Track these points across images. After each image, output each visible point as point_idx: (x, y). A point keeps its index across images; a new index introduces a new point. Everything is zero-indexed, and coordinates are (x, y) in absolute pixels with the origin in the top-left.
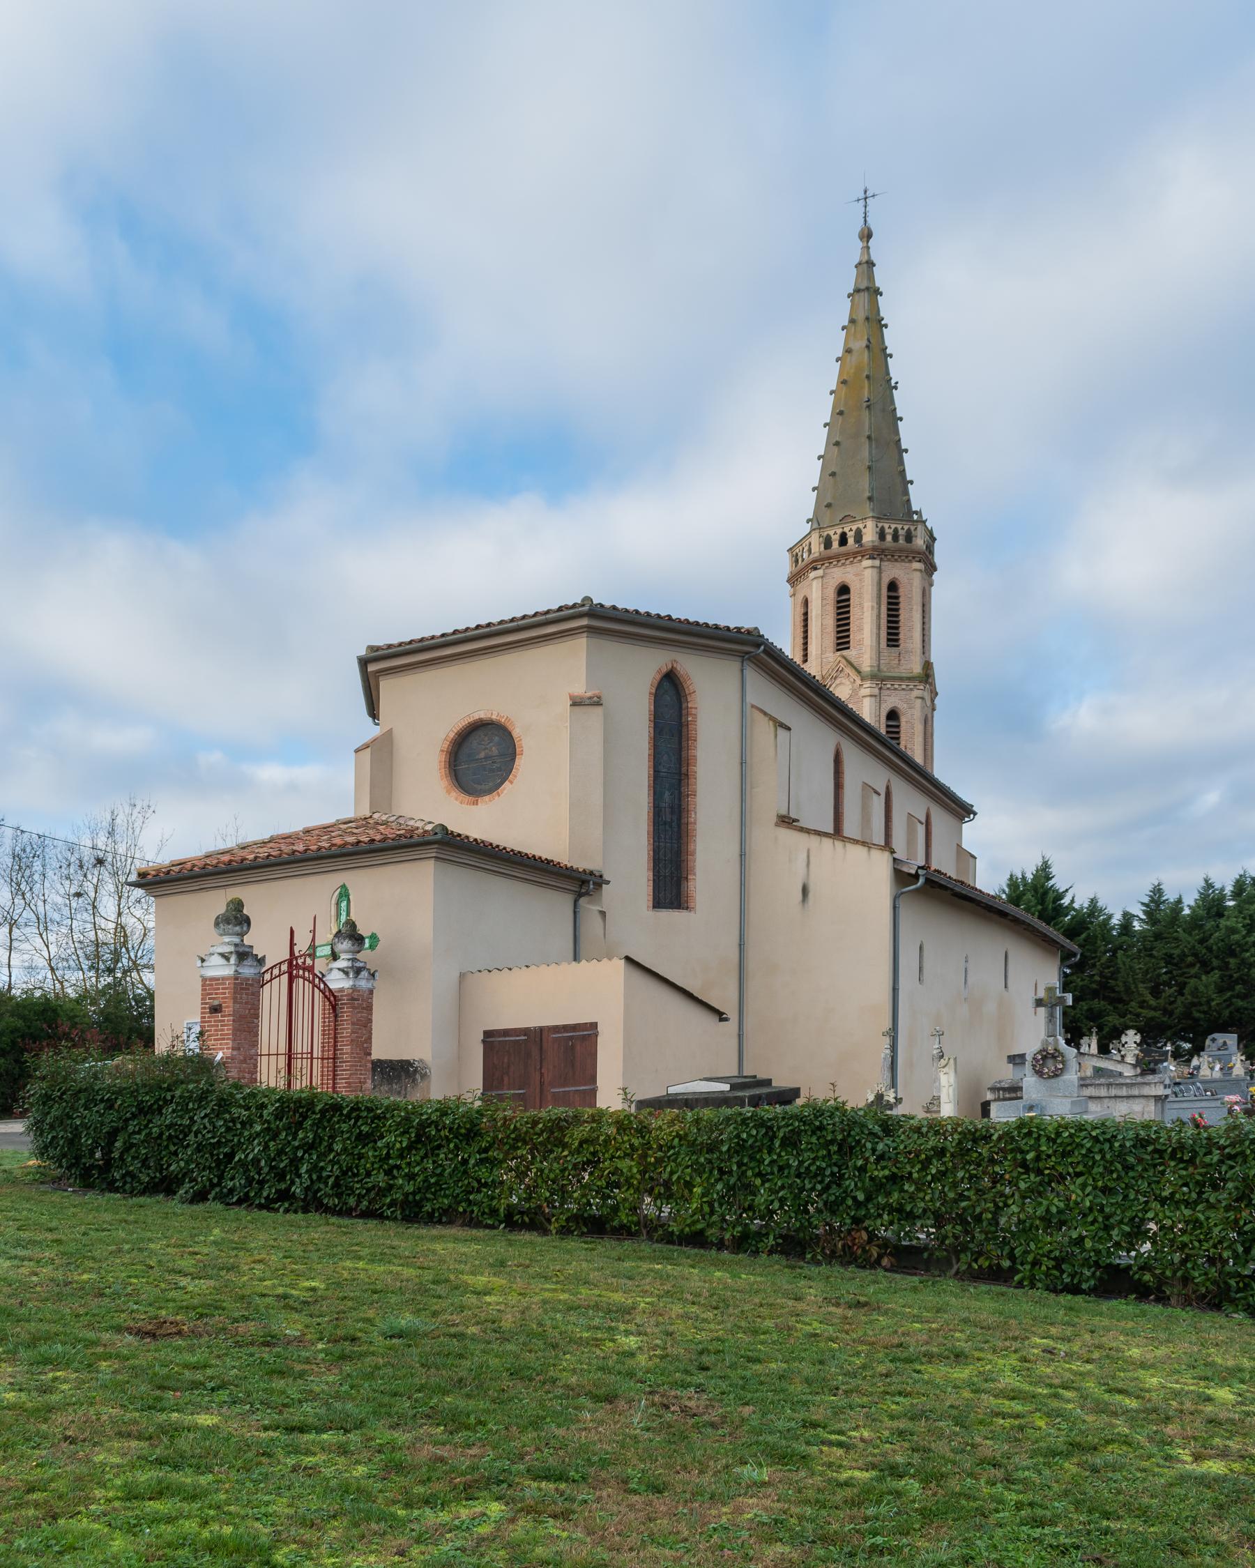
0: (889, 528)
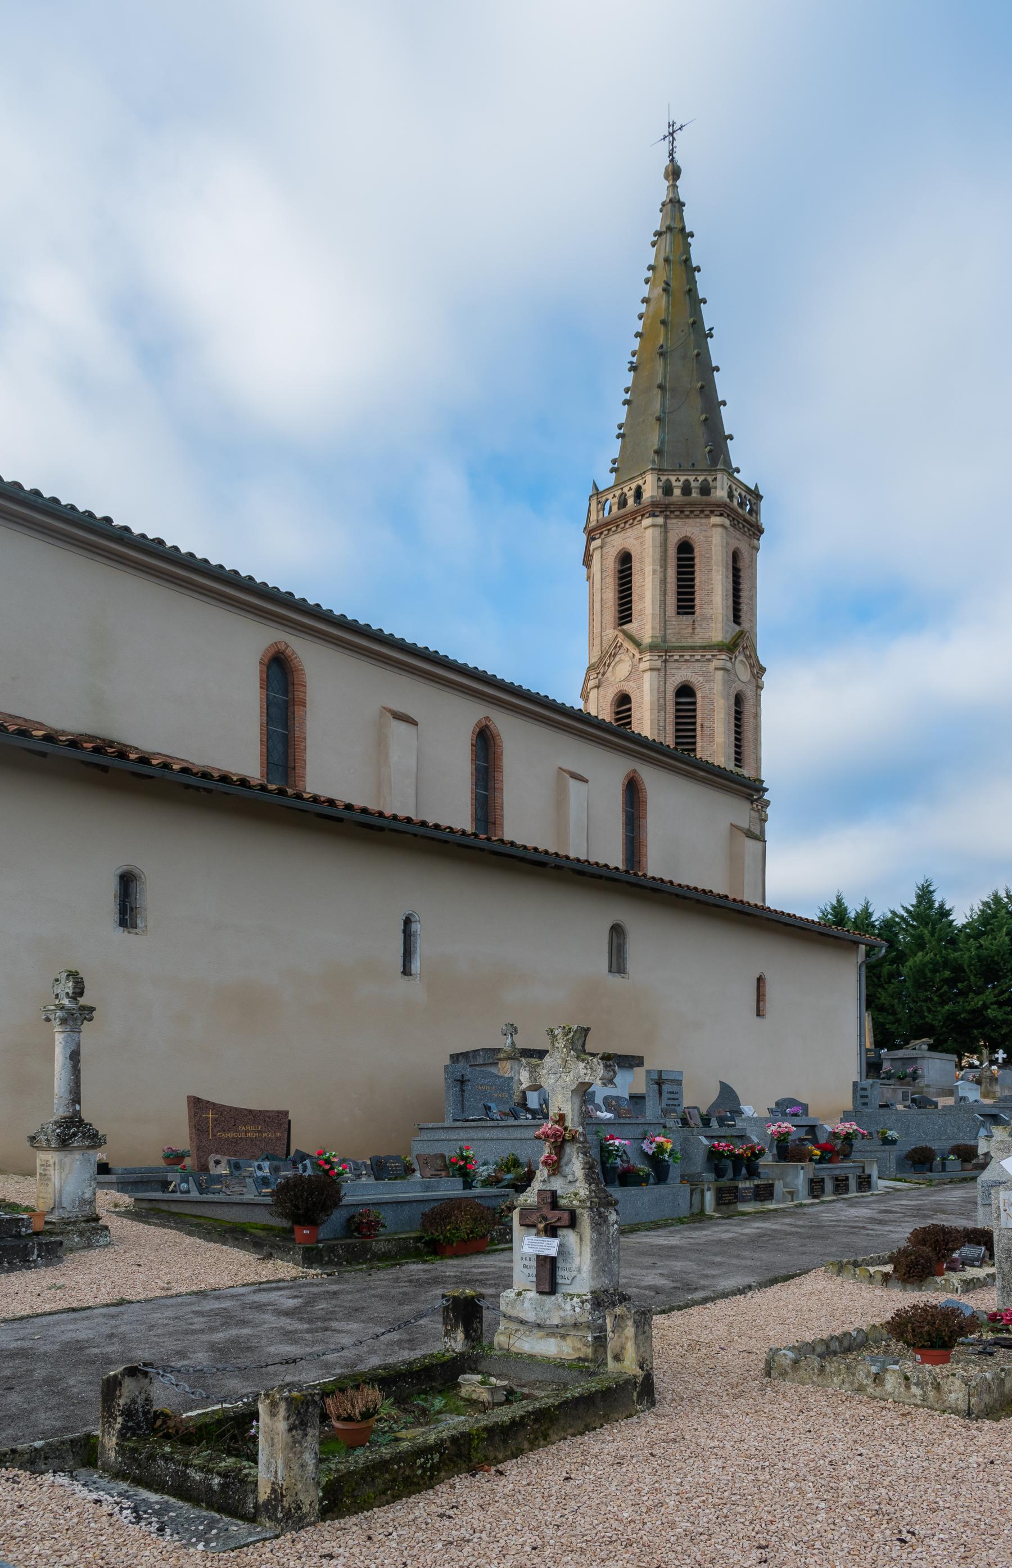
0: (677, 482)
